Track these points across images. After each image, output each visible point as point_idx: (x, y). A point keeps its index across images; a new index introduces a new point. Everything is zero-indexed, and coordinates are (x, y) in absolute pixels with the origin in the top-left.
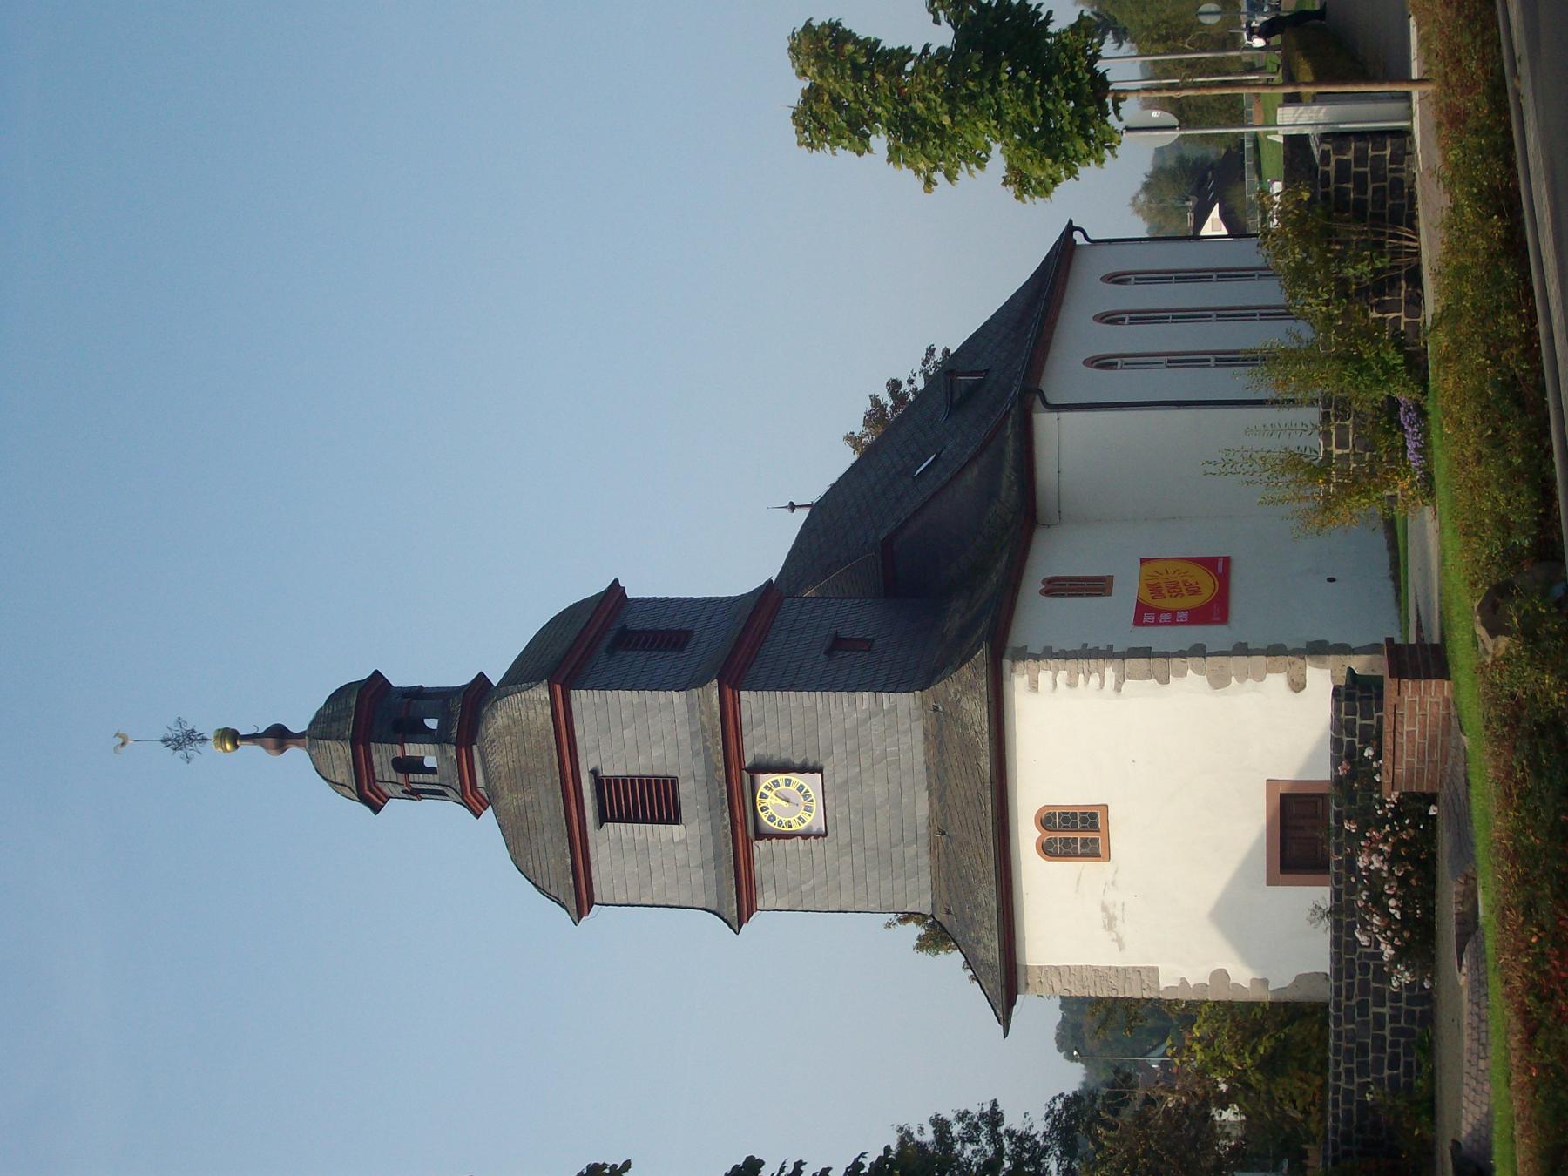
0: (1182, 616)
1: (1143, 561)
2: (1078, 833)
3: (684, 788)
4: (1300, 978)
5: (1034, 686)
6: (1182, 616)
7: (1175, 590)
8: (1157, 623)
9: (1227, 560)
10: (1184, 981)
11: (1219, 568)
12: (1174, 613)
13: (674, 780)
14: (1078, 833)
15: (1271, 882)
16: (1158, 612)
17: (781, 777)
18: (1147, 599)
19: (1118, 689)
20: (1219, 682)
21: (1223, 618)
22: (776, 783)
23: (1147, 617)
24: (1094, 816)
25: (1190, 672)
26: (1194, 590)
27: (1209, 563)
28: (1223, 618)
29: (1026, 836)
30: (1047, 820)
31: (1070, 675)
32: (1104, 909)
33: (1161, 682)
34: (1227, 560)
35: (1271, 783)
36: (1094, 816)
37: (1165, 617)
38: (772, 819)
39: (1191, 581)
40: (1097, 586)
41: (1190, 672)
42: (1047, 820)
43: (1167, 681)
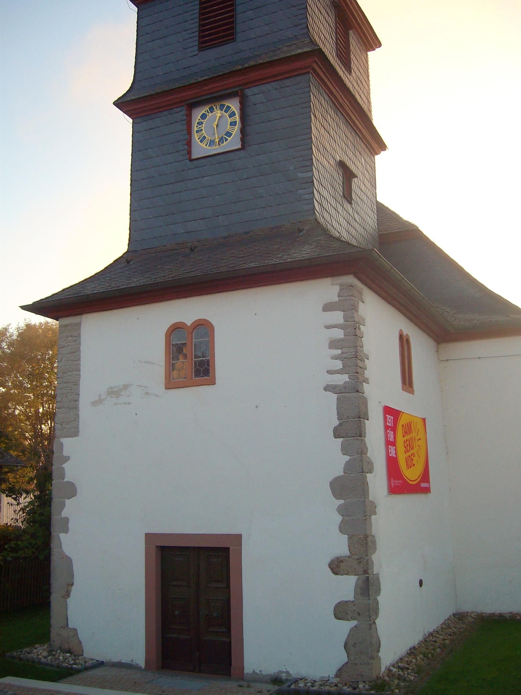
0: (392, 449)
1: (424, 420)
2: (192, 360)
3: (227, 49)
4: (69, 561)
5: (328, 307)
6: (392, 454)
7: (409, 446)
8: (387, 428)
9: (427, 490)
10: (67, 459)
11: (421, 487)
12: (394, 444)
13: (233, 40)
14: (192, 360)
15: (149, 537)
16: (394, 429)
17: (237, 118)
18: (403, 421)
19: (327, 388)
20: (71, 490)
21: (393, 490)
22: (233, 114)
23: (390, 418)
24: (226, 550)
25: (347, 458)
26: (410, 464)
27: (425, 476)
28: (393, 490)
29: (187, 311)
30: (204, 327)
31: (342, 340)
32: (126, 387)
33: (335, 430)
34: (427, 490)
35: (238, 538)
36: (226, 550)
37: (391, 434)
38: (204, 116)
39: (415, 459)
40: (407, 381)
41: (347, 458)
42: (204, 327)
43: (336, 436)
